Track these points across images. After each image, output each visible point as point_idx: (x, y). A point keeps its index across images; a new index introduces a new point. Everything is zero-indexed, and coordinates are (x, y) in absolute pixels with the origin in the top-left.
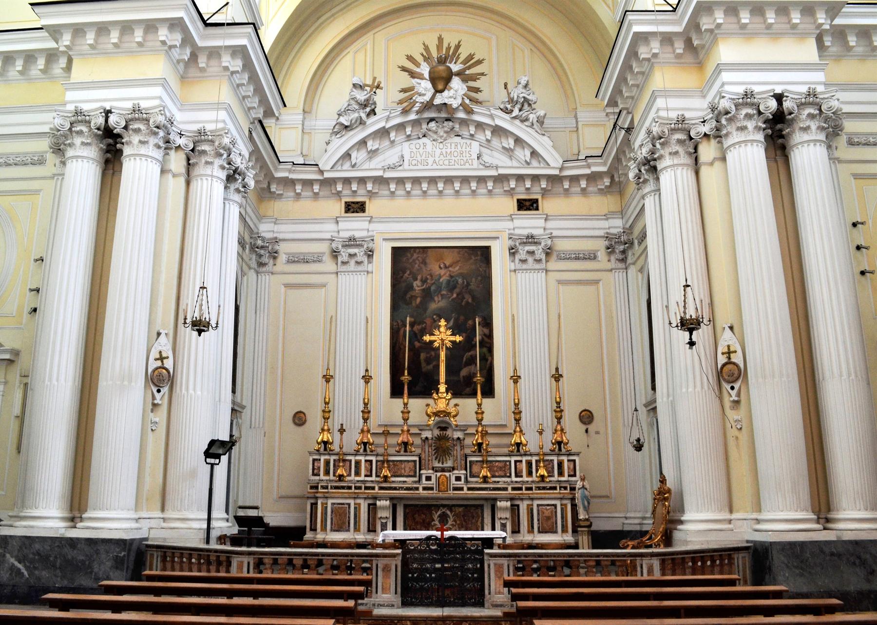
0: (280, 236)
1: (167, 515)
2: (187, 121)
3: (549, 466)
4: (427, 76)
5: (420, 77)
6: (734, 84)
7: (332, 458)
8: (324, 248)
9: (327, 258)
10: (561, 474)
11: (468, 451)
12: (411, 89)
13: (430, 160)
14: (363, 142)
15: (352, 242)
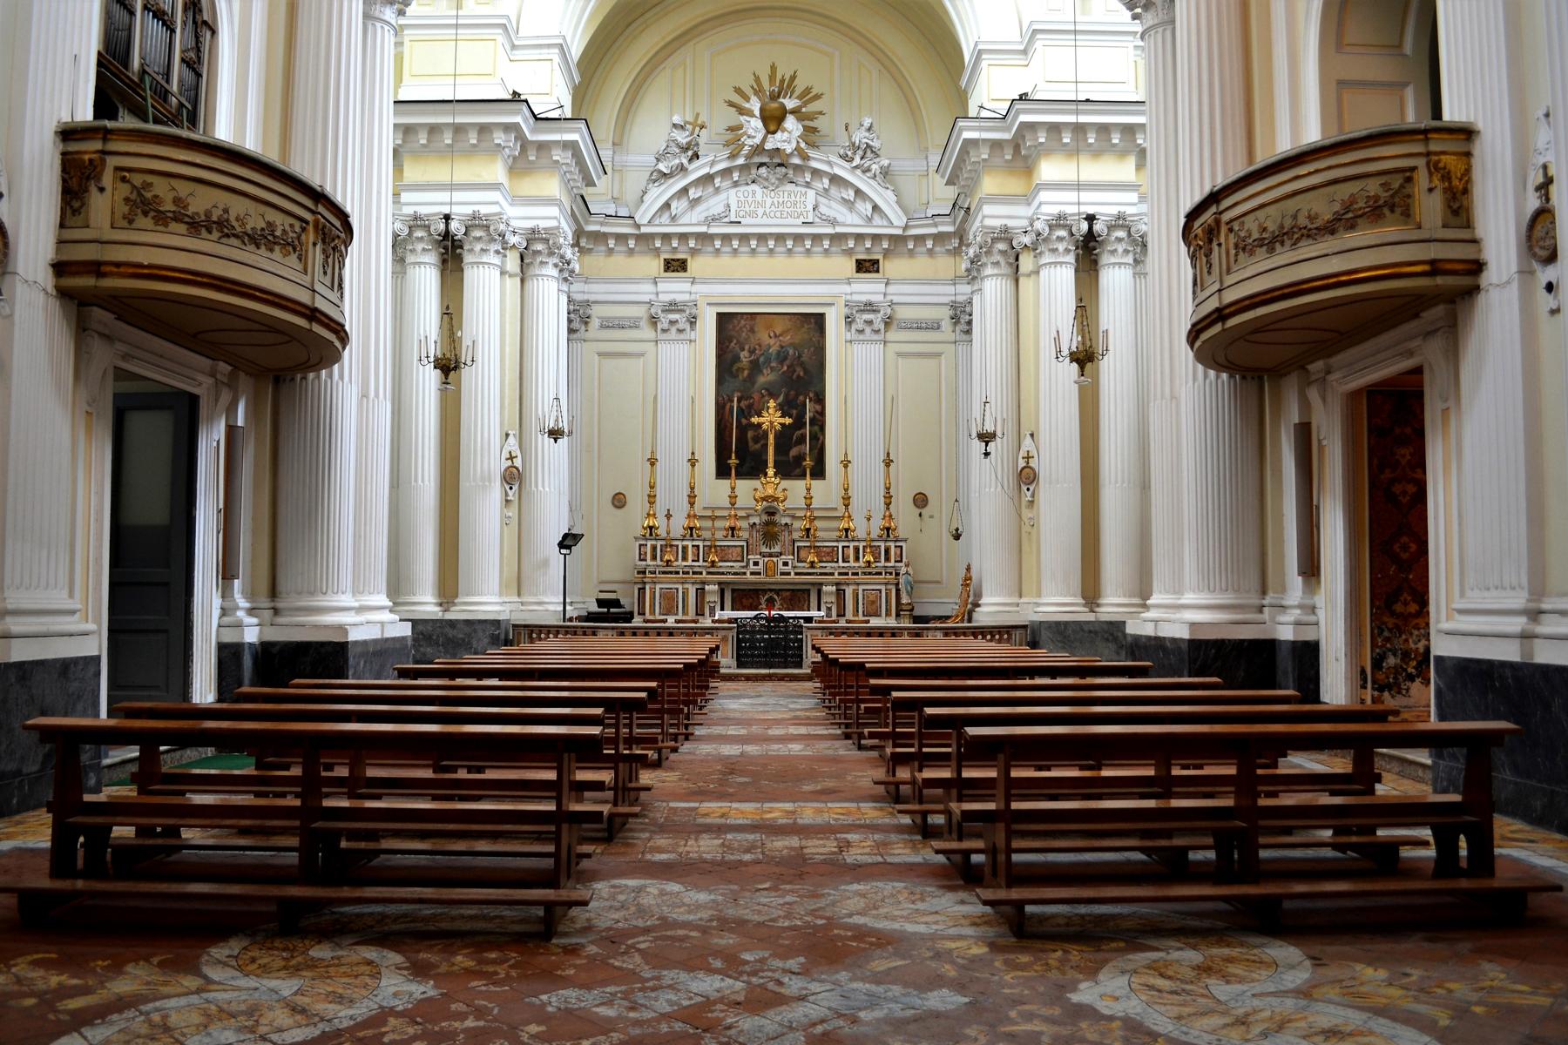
0: (592, 298)
1: (525, 599)
2: (520, 219)
3: (875, 552)
4: (757, 113)
5: (750, 114)
6: (1052, 203)
7: (659, 544)
8: (640, 312)
9: (644, 323)
10: (887, 559)
11: (796, 535)
12: (740, 127)
13: (760, 211)
14: (685, 190)
15: (672, 307)
